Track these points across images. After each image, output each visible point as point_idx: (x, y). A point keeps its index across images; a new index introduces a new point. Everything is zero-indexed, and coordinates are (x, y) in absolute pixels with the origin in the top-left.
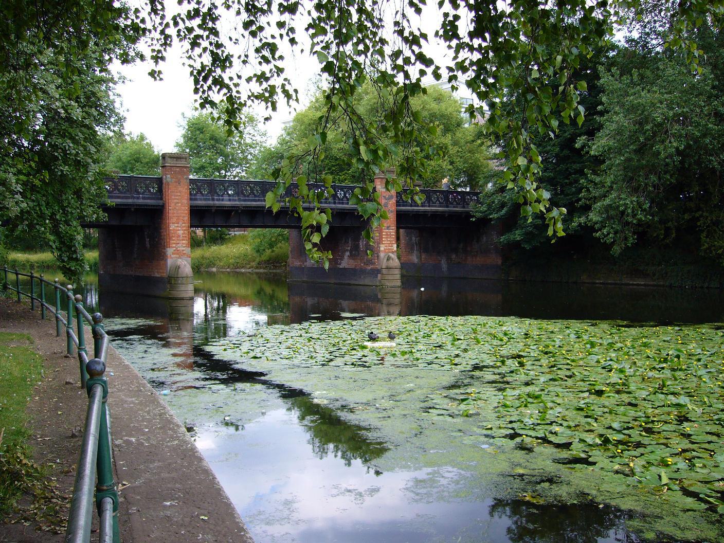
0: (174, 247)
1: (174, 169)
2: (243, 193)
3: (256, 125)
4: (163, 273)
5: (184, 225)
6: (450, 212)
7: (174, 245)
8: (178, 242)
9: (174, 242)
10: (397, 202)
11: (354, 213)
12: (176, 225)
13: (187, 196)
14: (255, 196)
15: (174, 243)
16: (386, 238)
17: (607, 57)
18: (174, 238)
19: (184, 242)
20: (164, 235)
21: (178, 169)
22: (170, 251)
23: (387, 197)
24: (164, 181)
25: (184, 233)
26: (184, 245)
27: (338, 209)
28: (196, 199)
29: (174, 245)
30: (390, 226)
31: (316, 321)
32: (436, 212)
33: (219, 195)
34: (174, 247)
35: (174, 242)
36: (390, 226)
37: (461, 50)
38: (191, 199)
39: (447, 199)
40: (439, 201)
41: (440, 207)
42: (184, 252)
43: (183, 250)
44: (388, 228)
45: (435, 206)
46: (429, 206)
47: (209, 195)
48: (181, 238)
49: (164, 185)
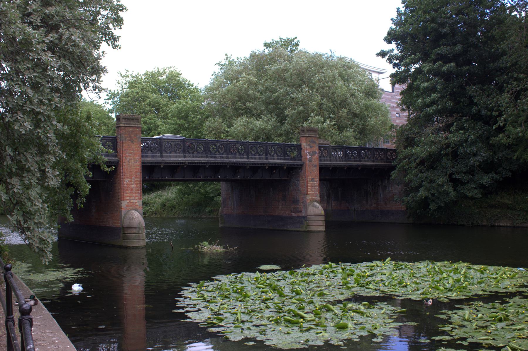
0: (127, 200)
1: (127, 129)
2: (210, 151)
3: (110, 91)
4: (118, 223)
5: (136, 179)
6: (376, 166)
7: (128, 198)
8: (131, 195)
9: (128, 195)
10: (320, 157)
11: (283, 167)
12: (129, 180)
13: (139, 153)
14: (199, 153)
15: (128, 196)
16: (311, 189)
17: (396, 28)
18: (128, 192)
19: (137, 195)
20: (119, 189)
21: (137, 130)
22: (124, 204)
23: (311, 153)
24: (119, 140)
25: (137, 187)
26: (137, 198)
27: (251, 164)
28: (147, 156)
29: (128, 198)
30: (314, 179)
31: (274, 267)
32: (366, 166)
33: (271, 155)
34: (127, 200)
35: (128, 195)
36: (314, 179)
37: (403, 10)
38: (143, 156)
39: (359, 154)
40: (353, 156)
41: (355, 161)
42: (137, 204)
43: (136, 203)
44: (312, 180)
45: (351, 161)
46: (330, 161)
47: (204, 153)
48: (133, 192)
49: (118, 144)
